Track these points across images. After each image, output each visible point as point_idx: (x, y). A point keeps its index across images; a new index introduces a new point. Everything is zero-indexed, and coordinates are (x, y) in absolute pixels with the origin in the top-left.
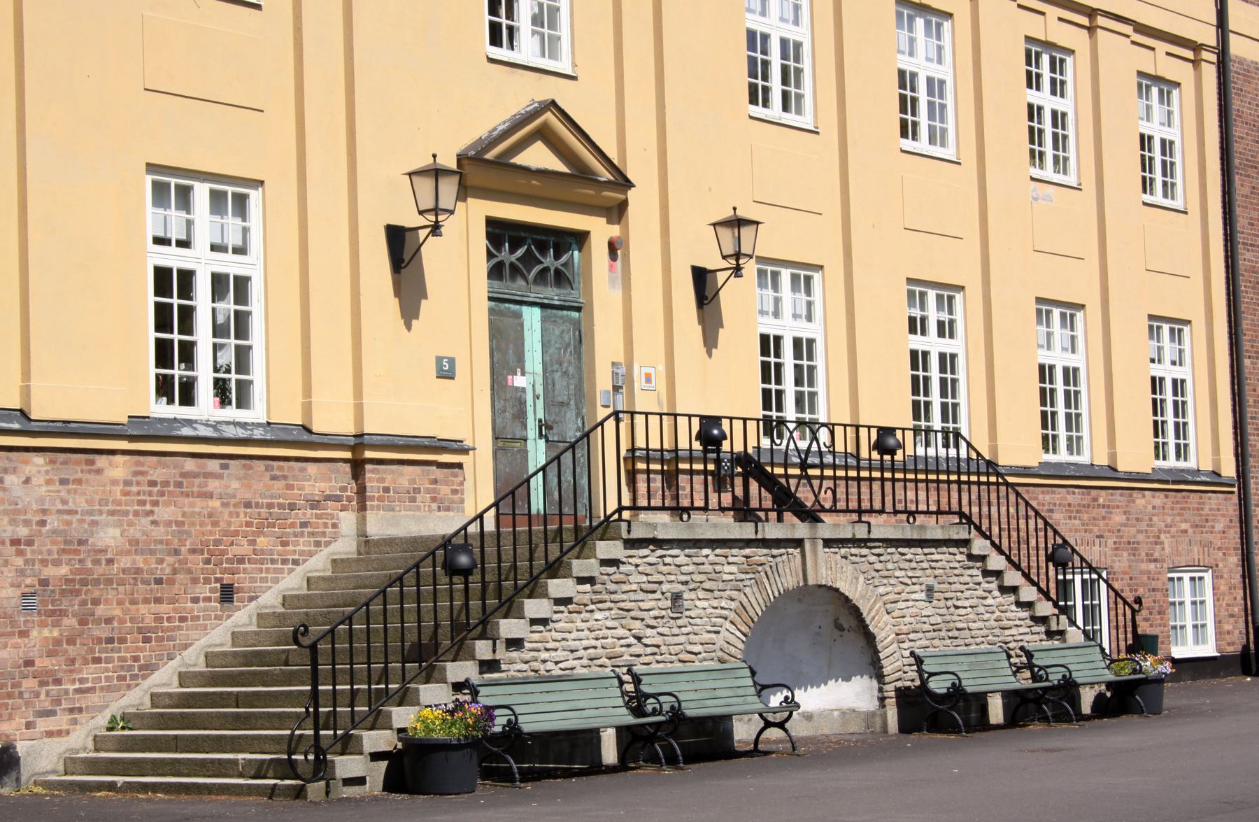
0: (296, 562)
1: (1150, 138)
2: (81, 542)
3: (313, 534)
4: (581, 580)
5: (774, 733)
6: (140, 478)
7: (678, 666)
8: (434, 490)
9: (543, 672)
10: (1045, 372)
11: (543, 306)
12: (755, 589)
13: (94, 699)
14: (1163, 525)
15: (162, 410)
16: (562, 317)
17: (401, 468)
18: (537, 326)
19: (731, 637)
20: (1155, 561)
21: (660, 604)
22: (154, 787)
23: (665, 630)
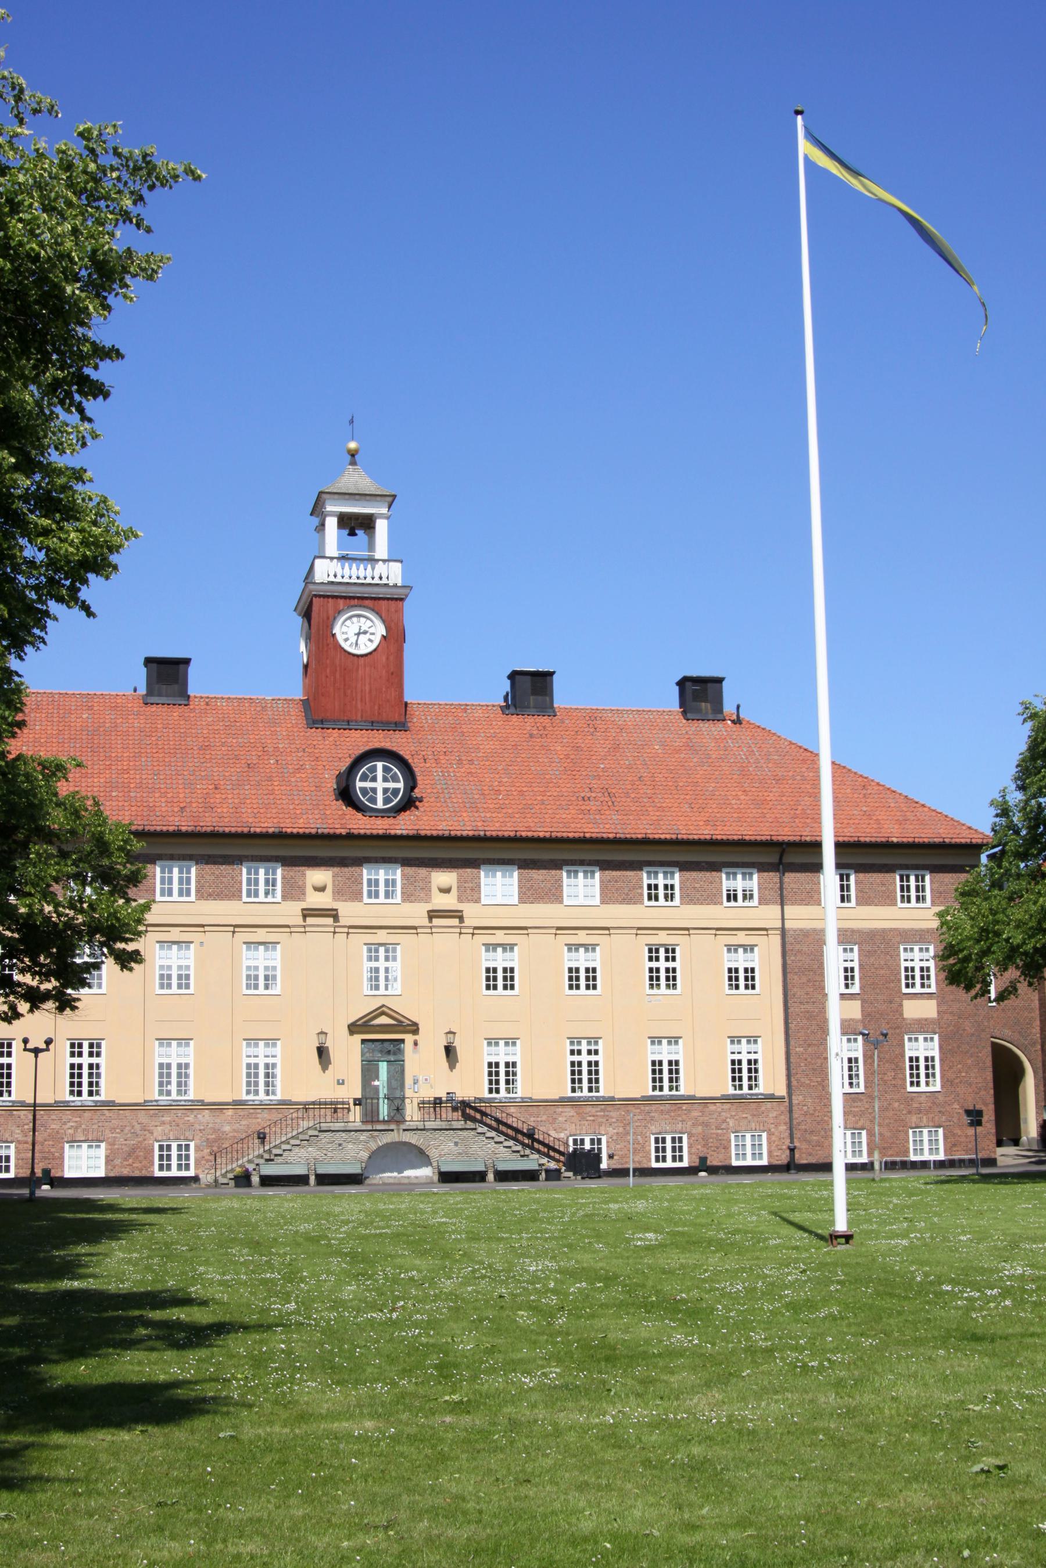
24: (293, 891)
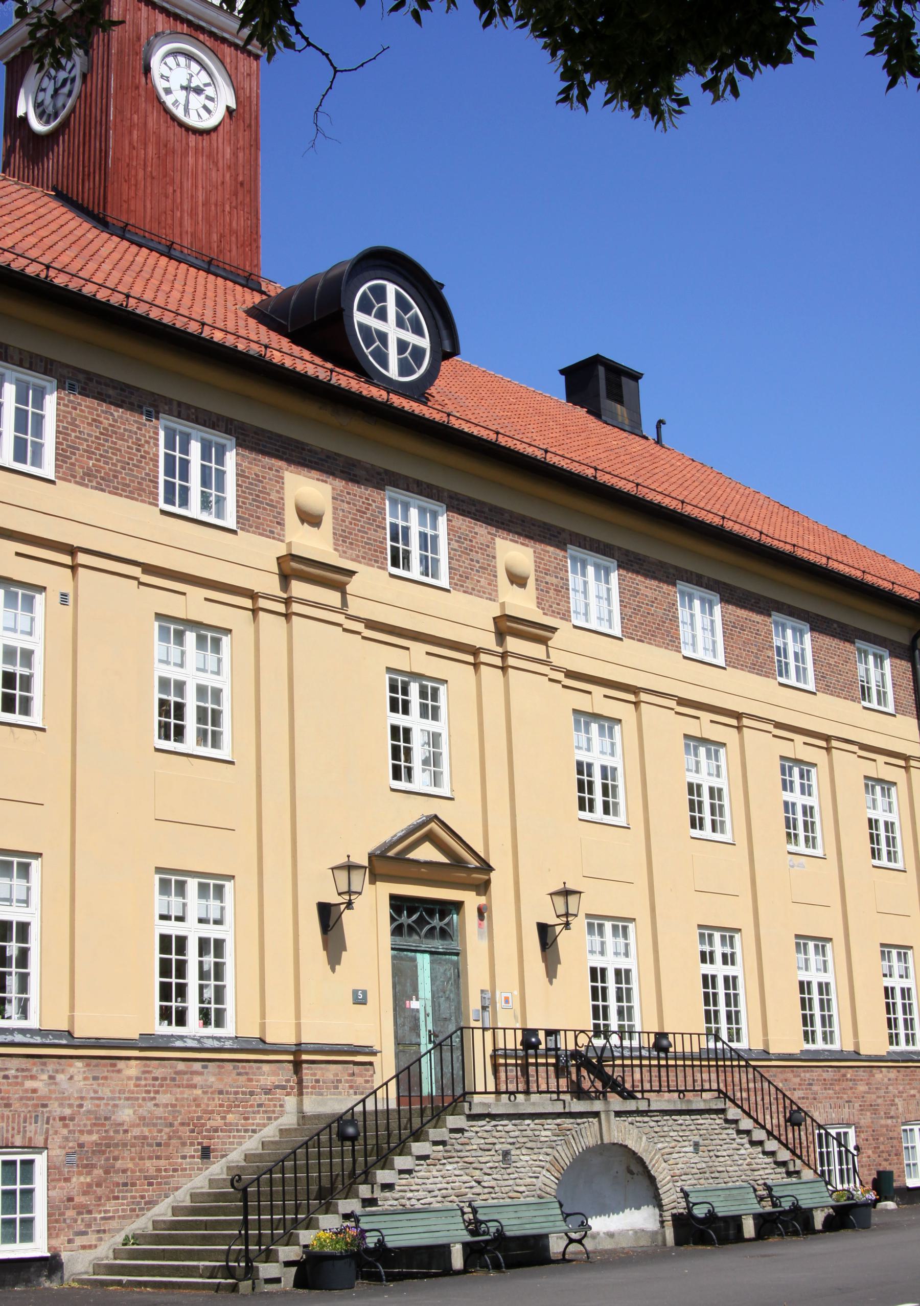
0: (254, 1131)
1: (876, 821)
2: (106, 1119)
3: (266, 1112)
4: (436, 1143)
5: (574, 1247)
6: (147, 1075)
7: (508, 1201)
8: (351, 1081)
9: (408, 1206)
10: (804, 987)
11: (432, 953)
12: (565, 1147)
13: (114, 1224)
14: (896, 1092)
15: (165, 1029)
16: (445, 960)
17: (328, 1066)
18: (427, 966)
19: (548, 1180)
20: (892, 1117)
21: (494, 1158)
22: (146, 1284)
23: (498, 1177)
24: (260, 514)
